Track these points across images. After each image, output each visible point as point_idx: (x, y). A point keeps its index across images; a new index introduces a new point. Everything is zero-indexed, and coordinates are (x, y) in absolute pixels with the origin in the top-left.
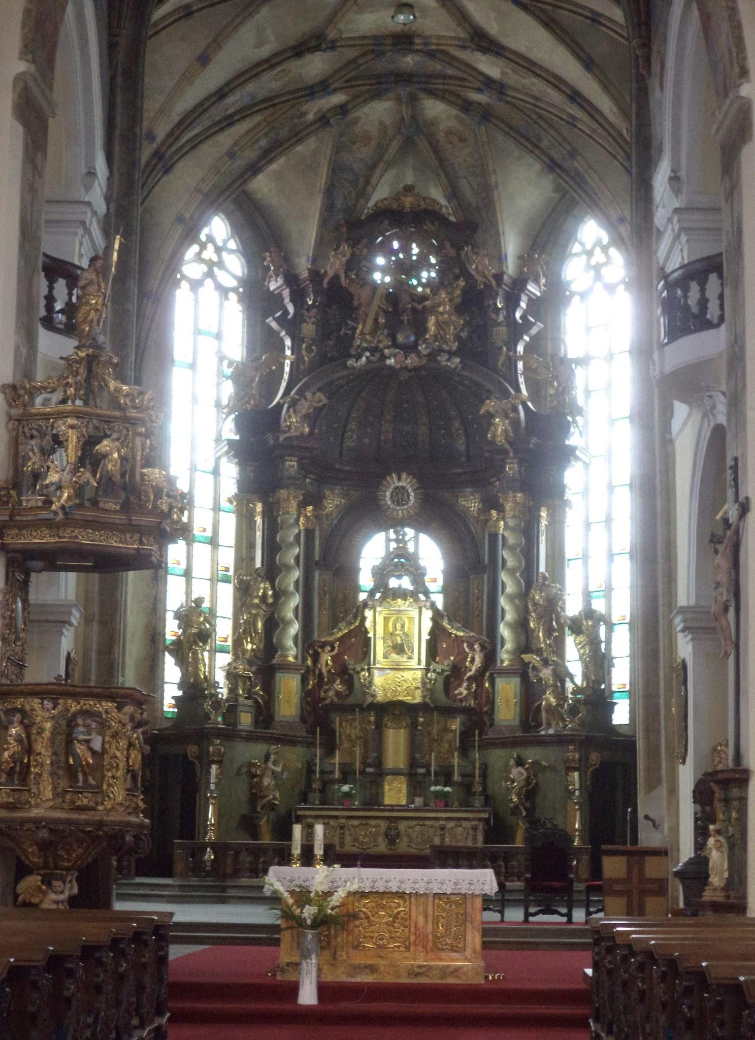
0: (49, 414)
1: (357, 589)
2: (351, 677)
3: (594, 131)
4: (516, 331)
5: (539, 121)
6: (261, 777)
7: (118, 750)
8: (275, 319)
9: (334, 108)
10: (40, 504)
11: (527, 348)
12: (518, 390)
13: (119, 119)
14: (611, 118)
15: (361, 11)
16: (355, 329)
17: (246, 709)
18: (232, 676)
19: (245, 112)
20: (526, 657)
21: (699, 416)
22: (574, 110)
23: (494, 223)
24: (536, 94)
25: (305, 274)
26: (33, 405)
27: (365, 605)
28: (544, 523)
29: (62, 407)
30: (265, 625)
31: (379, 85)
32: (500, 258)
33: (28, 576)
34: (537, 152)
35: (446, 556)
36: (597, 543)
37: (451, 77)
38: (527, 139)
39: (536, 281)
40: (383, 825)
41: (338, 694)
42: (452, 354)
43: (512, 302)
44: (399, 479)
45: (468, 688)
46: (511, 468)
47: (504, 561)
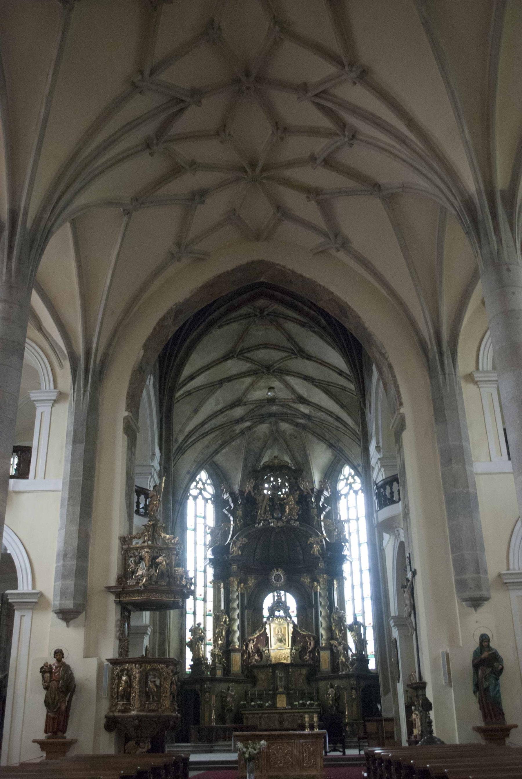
0: (138, 547)
1: (262, 617)
2: (261, 653)
3: (346, 431)
4: (320, 510)
5: (325, 429)
6: (226, 697)
7: (167, 685)
8: (226, 510)
9: (246, 428)
10: (134, 584)
11: (325, 517)
12: (322, 533)
13: (164, 433)
14: (352, 426)
15: (255, 391)
16: (257, 512)
17: (219, 668)
18: (213, 654)
19: (212, 430)
20: (332, 642)
21: (394, 537)
22: (337, 424)
23: (310, 469)
24: (323, 418)
25: (237, 492)
26: (132, 544)
27: (266, 623)
28: (335, 586)
29: (143, 545)
30: (226, 633)
31: (263, 419)
32: (312, 482)
33: (130, 614)
34: (324, 441)
35: (297, 602)
36: (357, 597)
37: (291, 414)
38: (321, 437)
39: (327, 490)
40: (277, 716)
41: (256, 660)
42: (295, 520)
43: (318, 499)
44: (277, 571)
45: (309, 656)
46: (321, 565)
47: (321, 612)
